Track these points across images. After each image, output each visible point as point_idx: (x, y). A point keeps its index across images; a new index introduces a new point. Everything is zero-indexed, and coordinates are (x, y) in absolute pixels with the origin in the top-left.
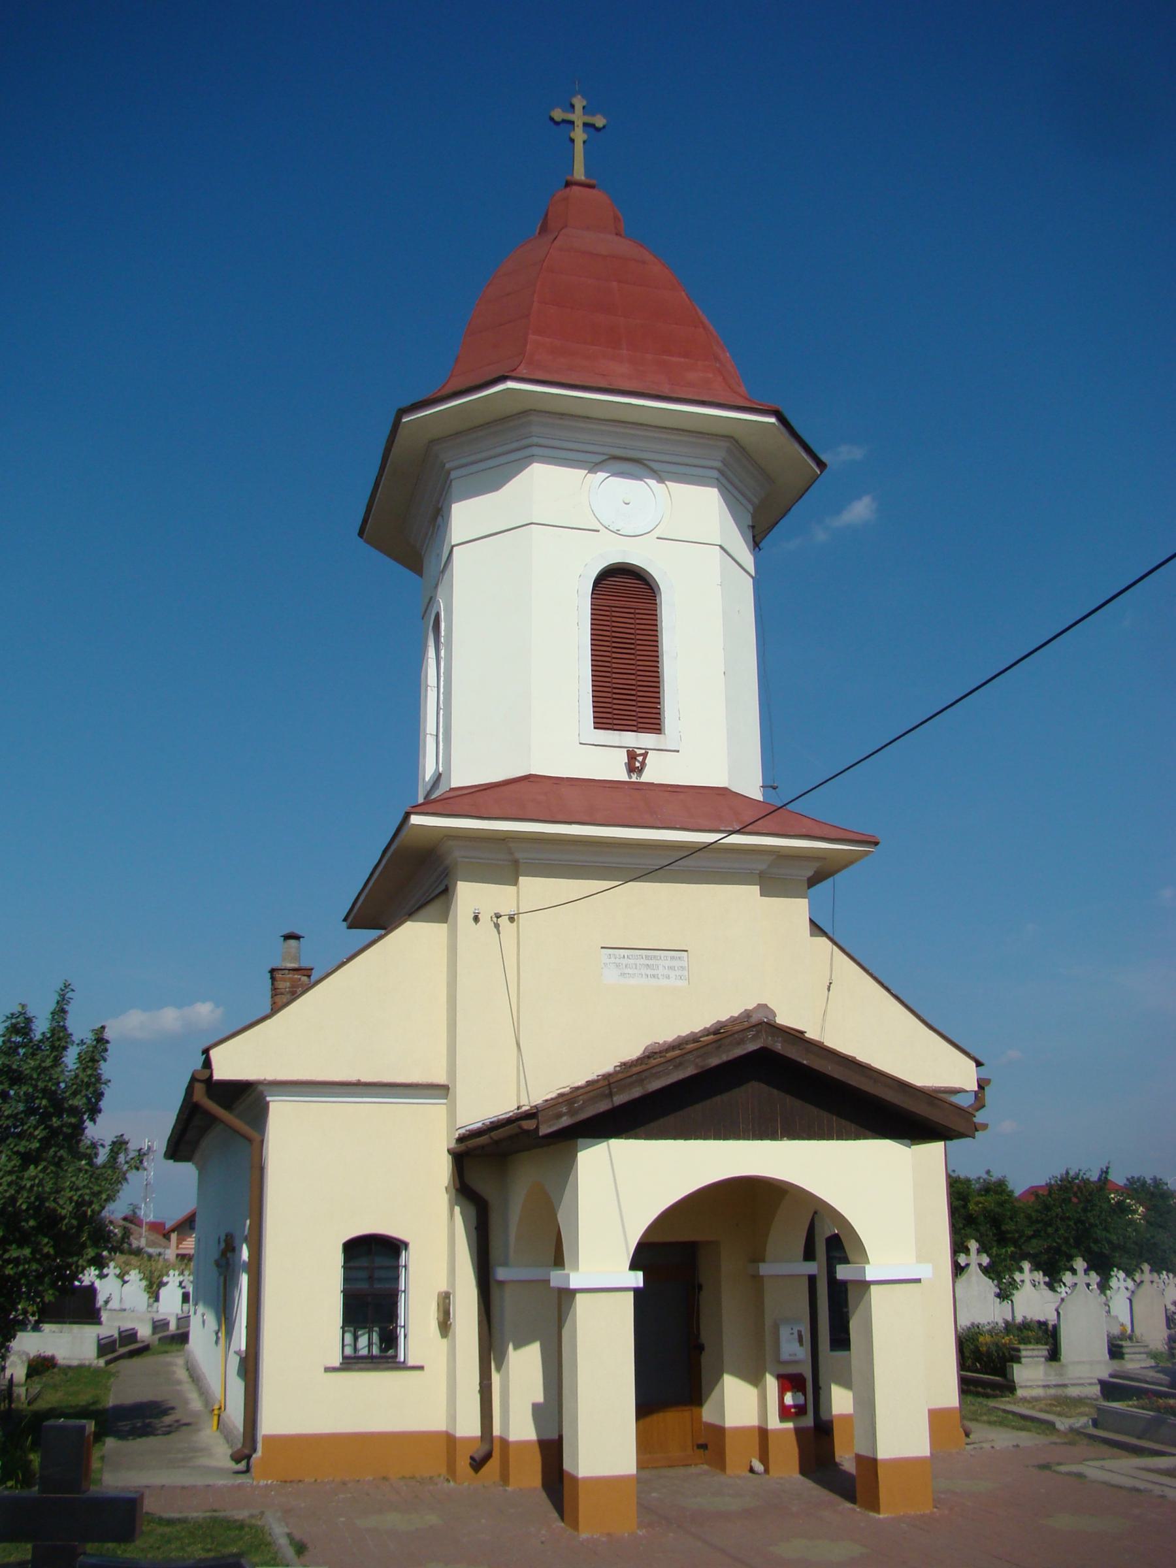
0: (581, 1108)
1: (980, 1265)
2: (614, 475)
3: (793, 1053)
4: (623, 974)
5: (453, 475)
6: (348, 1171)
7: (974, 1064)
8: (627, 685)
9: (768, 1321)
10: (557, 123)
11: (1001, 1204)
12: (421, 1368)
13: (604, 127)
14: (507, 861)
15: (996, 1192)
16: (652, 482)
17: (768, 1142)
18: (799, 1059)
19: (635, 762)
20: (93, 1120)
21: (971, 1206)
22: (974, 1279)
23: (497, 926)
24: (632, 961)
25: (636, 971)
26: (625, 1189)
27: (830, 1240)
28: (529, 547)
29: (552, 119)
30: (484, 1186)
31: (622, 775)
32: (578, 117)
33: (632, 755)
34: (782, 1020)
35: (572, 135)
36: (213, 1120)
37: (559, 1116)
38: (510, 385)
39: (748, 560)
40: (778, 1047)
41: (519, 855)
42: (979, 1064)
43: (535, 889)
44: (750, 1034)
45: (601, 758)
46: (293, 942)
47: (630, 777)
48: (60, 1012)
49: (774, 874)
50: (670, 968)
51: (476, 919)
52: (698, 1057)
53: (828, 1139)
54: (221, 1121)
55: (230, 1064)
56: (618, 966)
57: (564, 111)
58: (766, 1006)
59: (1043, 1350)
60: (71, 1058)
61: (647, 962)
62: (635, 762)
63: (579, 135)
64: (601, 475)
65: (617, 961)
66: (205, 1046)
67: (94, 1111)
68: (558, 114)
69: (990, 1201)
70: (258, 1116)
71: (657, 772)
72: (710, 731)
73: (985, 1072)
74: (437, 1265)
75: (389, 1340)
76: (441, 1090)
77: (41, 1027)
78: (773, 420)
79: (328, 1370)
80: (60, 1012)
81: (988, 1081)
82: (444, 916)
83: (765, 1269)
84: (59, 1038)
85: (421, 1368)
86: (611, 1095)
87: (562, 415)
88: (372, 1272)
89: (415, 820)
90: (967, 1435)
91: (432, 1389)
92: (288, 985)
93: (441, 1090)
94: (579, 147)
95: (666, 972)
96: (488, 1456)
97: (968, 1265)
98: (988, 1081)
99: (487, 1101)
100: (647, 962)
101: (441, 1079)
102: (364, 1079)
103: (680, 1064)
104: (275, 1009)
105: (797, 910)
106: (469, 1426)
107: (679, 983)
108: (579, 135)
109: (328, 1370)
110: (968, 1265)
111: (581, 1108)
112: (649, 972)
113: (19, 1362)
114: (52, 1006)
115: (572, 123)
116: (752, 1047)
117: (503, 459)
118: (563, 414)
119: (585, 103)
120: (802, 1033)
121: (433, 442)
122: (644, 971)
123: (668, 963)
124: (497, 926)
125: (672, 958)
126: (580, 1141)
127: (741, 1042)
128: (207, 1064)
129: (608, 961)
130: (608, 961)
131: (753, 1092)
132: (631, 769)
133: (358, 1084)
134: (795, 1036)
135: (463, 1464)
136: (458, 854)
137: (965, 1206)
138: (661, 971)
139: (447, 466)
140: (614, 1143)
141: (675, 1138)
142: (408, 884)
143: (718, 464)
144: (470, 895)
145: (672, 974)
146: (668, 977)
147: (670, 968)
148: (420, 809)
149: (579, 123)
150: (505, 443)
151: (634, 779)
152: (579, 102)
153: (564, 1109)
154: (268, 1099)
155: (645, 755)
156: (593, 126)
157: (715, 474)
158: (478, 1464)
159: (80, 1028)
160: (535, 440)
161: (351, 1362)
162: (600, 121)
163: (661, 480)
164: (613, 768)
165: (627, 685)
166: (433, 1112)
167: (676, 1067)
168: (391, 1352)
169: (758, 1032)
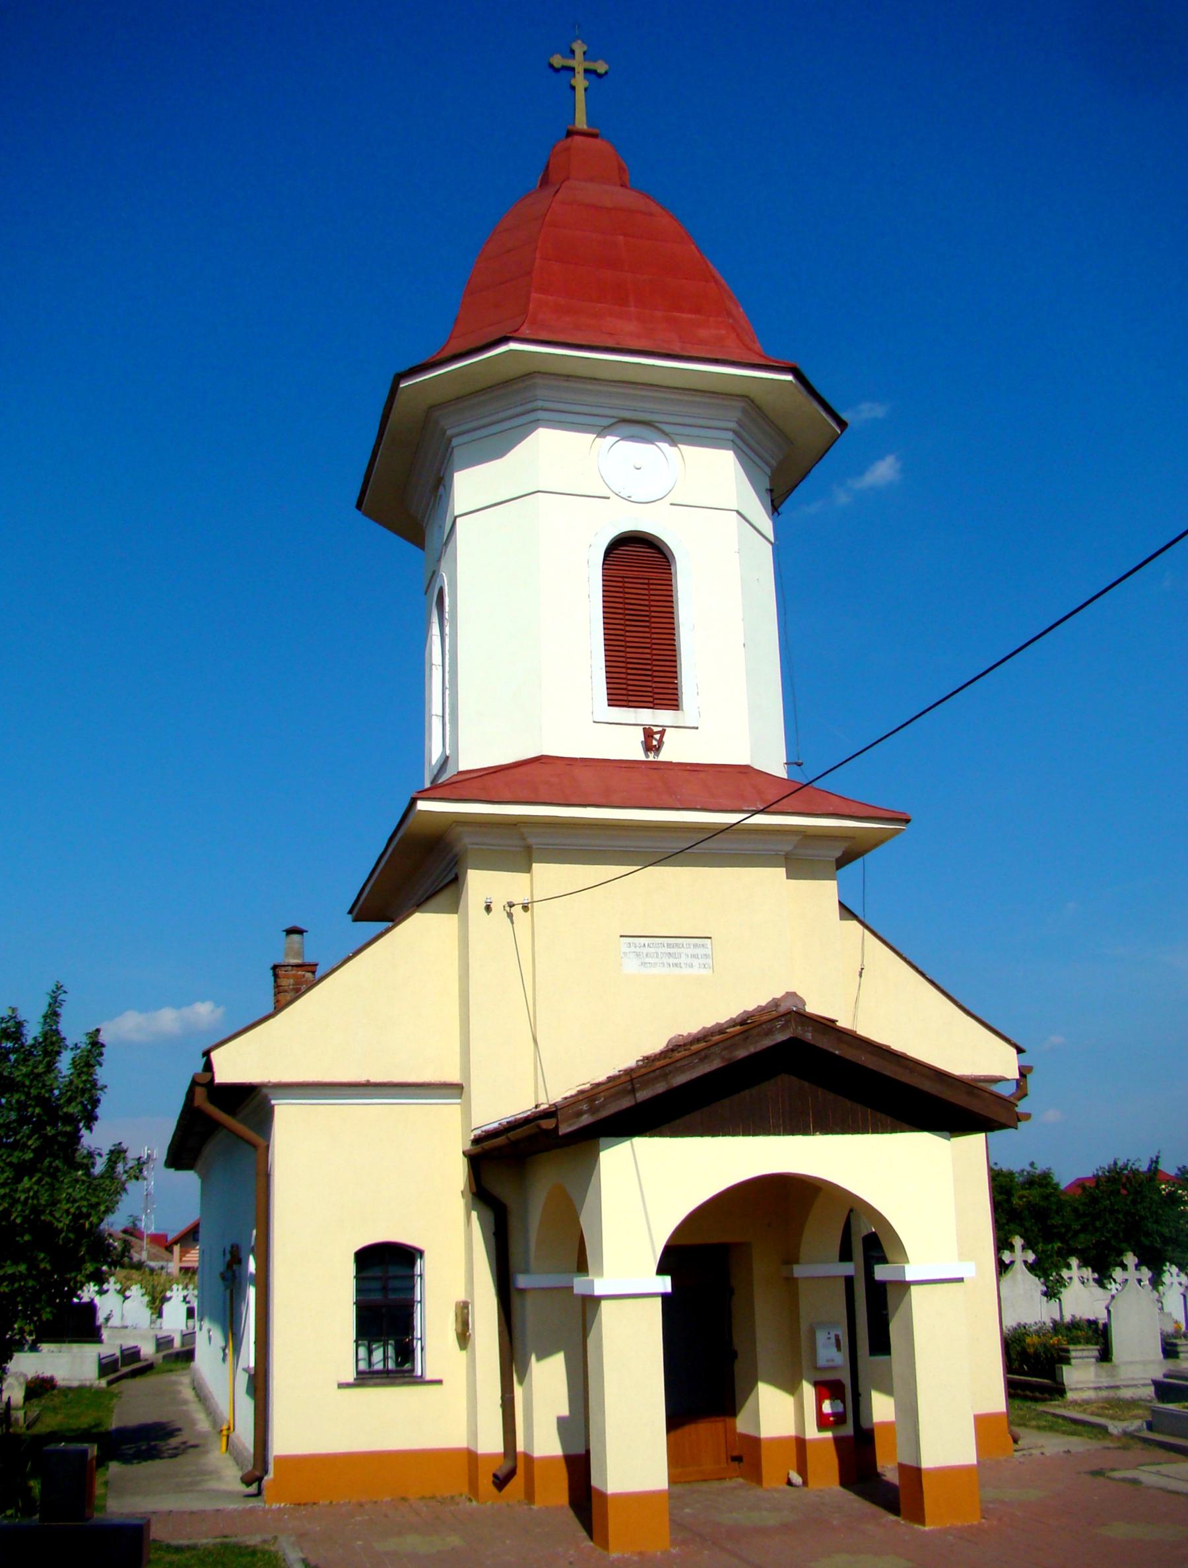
0: (603, 1105)
1: (1025, 1262)
2: (624, 438)
3: (824, 1043)
4: (643, 964)
5: (455, 442)
6: (358, 1178)
7: (1015, 1051)
8: (642, 660)
9: (804, 1326)
10: (557, 70)
11: (1046, 1197)
12: (440, 1382)
13: (606, 73)
14: (520, 847)
15: (1041, 1185)
16: (664, 446)
17: (800, 1137)
18: (831, 1050)
19: (652, 739)
20: (90, 1128)
21: (1015, 1200)
22: (1019, 1277)
23: (510, 915)
24: (652, 950)
25: (657, 960)
26: (649, 1190)
27: (867, 1240)
28: (535, 516)
29: (551, 66)
30: (503, 1190)
31: (639, 754)
32: (579, 63)
33: (648, 733)
34: (810, 1009)
35: (573, 82)
36: (212, 1127)
37: (579, 1114)
38: (513, 346)
39: (766, 524)
40: (809, 1036)
41: (531, 841)
42: (1020, 1051)
43: (549, 876)
44: (779, 1024)
45: (616, 737)
46: (295, 937)
47: (647, 756)
48: (53, 1015)
49: (800, 857)
50: (693, 956)
51: (488, 908)
52: (724, 1049)
53: (863, 1133)
54: (224, 1126)
55: (234, 1066)
56: (638, 955)
57: (564, 57)
58: (794, 994)
59: (1093, 1351)
60: (64, 1063)
61: (671, 950)
62: (652, 739)
63: (580, 82)
64: (610, 439)
65: (638, 950)
66: (205, 1047)
67: (90, 1119)
68: (557, 61)
69: (1034, 1194)
70: (263, 1120)
71: (674, 750)
72: (732, 701)
73: (1027, 1060)
74: (455, 1274)
75: (406, 1353)
76: (454, 1089)
77: (33, 1031)
78: (789, 378)
79: (341, 1386)
80: (53, 1015)
81: (1030, 1069)
82: (454, 906)
83: (799, 1271)
84: (52, 1042)
85: (440, 1382)
86: (633, 1091)
87: (568, 377)
88: (386, 1283)
89: (422, 805)
90: (1015, 1441)
91: (452, 1404)
92: (292, 982)
93: (454, 1089)
94: (580, 95)
95: (689, 960)
96: (512, 1473)
97: (1012, 1262)
98: (1030, 1069)
99: (503, 1101)
100: (671, 950)
101: (455, 1078)
102: (373, 1080)
103: (706, 1057)
104: (279, 1008)
105: (824, 893)
106: (491, 1443)
107: (704, 972)
108: (580, 82)
109: (341, 1386)
110: (1012, 1262)
111: (603, 1105)
112: (671, 961)
113: (16, 1383)
114: (44, 1009)
115: (572, 69)
116: (780, 1037)
117: (506, 425)
118: (568, 376)
119: (585, 48)
120: (834, 1021)
121: (432, 407)
122: (666, 960)
123: (690, 951)
124: (510, 915)
125: (695, 946)
126: (603, 1140)
127: (769, 1033)
128: (208, 1067)
129: (628, 950)
130: (628, 950)
131: (782, 1085)
132: (648, 747)
133: (368, 1085)
134: (827, 1026)
135: (486, 1483)
136: (467, 841)
137: (1008, 1201)
138: (683, 960)
139: (449, 433)
140: (638, 1141)
141: (702, 1134)
142: (415, 873)
143: (733, 425)
144: (481, 883)
145: (695, 962)
146: (691, 966)
147: (693, 956)
148: (426, 795)
149: (580, 69)
150: (509, 406)
151: (651, 758)
152: (579, 48)
153: (585, 1107)
154: (273, 1102)
155: (662, 733)
156: (594, 72)
157: (730, 435)
158: (501, 1482)
159: (73, 1031)
160: (540, 404)
161: (366, 1378)
162: (601, 67)
163: (674, 443)
164: (630, 748)
165: (642, 660)
166: (447, 1112)
167: (702, 1060)
168: (407, 1366)
169: (787, 1022)
